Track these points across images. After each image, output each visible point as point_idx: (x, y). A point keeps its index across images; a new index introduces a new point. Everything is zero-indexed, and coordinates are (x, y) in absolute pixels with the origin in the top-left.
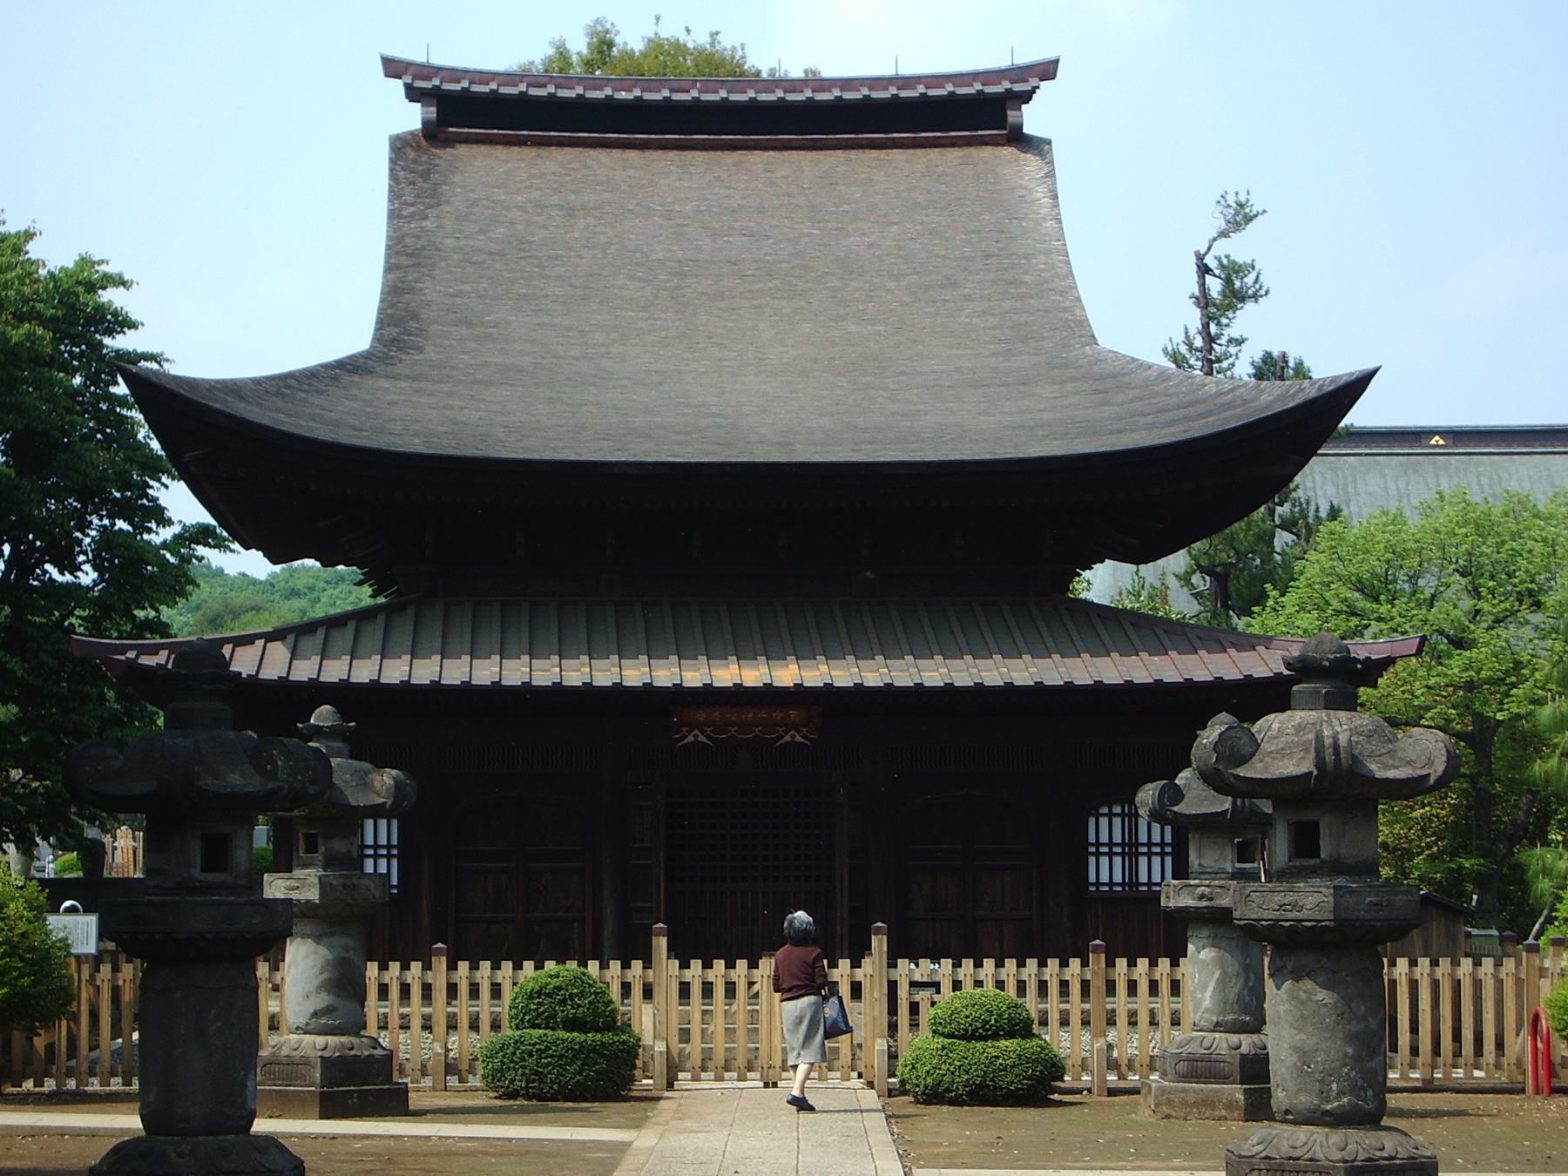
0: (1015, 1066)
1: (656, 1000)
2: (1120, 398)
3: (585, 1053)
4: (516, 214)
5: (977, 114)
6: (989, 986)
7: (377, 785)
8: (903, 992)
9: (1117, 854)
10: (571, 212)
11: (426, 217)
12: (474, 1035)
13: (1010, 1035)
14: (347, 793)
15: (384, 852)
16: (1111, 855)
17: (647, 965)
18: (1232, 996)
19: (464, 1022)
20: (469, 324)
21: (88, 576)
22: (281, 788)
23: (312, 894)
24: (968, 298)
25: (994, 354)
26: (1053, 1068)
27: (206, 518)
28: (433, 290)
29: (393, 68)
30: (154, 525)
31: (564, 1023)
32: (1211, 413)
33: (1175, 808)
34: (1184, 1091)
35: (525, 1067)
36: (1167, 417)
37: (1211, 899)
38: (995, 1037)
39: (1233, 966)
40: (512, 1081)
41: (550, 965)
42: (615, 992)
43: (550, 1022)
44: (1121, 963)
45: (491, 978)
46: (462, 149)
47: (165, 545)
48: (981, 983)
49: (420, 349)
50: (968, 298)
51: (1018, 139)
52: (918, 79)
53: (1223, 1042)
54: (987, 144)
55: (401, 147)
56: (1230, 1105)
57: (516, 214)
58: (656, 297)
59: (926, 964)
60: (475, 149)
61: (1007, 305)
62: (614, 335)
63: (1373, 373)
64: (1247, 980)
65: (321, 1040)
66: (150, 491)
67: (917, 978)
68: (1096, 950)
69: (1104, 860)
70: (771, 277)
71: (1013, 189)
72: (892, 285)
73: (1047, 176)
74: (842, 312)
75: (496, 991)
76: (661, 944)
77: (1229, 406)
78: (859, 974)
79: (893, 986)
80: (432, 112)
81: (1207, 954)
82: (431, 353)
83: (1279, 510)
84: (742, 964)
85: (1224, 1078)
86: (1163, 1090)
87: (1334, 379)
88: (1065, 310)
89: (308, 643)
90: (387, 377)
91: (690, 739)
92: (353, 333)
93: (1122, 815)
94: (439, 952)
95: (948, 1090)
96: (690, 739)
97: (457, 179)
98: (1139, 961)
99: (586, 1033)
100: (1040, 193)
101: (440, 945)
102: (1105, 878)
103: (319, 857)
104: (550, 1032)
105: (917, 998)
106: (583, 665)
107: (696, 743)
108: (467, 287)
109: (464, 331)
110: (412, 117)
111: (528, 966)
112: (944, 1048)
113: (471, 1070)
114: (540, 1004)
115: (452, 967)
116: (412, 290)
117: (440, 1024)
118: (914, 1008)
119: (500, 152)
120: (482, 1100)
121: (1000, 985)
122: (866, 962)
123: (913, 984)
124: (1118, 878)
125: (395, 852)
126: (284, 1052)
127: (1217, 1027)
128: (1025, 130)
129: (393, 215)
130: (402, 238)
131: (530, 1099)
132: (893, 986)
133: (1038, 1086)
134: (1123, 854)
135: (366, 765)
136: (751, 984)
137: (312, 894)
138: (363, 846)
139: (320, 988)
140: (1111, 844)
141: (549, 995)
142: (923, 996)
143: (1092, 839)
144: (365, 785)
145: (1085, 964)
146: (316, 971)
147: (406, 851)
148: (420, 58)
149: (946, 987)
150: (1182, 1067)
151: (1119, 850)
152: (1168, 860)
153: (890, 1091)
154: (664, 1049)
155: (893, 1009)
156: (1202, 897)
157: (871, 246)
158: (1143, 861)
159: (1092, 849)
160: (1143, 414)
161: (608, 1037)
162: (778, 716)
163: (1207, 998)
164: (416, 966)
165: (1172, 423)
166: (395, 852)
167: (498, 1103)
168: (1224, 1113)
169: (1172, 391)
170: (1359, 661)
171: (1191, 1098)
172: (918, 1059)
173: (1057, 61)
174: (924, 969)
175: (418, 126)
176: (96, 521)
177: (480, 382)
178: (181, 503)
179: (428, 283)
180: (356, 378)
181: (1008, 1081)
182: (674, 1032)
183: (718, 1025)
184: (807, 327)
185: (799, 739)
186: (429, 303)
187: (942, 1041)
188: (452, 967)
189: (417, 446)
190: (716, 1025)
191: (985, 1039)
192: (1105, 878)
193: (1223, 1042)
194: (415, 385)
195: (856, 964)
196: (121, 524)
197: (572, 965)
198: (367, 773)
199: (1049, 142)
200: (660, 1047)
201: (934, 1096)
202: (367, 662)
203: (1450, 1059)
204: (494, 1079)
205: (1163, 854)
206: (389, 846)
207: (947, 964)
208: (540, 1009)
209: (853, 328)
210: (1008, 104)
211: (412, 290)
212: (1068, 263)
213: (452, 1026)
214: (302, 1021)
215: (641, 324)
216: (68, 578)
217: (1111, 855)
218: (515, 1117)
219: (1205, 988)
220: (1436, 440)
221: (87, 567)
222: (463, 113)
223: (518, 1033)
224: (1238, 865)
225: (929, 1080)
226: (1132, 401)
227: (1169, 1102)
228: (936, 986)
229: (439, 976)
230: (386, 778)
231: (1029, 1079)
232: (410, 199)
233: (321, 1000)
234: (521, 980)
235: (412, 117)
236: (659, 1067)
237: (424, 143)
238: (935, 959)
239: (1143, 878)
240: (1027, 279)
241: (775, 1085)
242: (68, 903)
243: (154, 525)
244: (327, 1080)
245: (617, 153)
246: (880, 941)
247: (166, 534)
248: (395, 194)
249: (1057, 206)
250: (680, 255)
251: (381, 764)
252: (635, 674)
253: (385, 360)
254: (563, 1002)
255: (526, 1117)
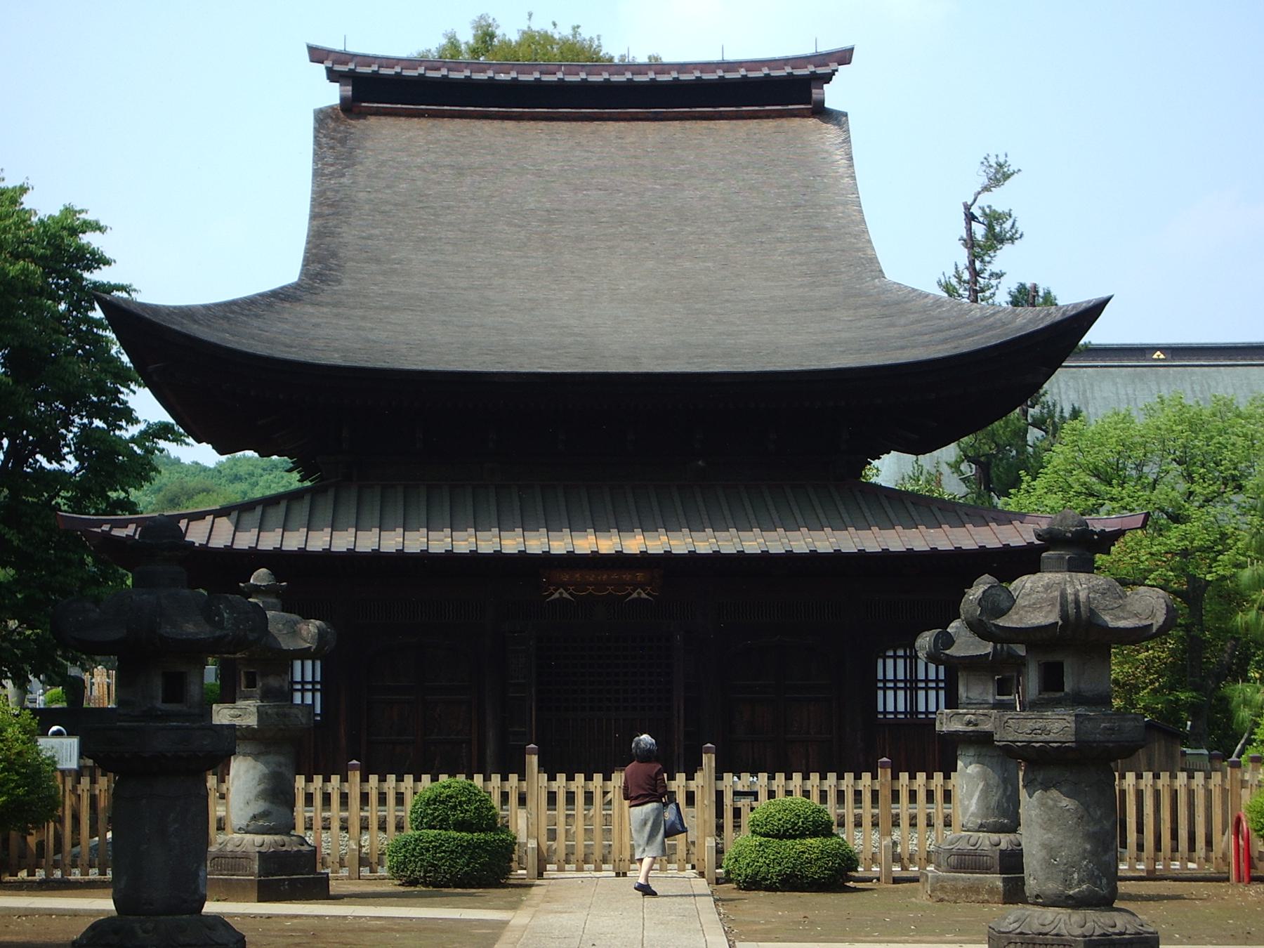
0: (818, 859)
1: (529, 806)
2: (903, 321)
3: (472, 849)
4: (416, 173)
5: (787, 92)
6: (798, 795)
7: (304, 633)
8: (728, 799)
9: (901, 688)
10: (460, 171)
11: (343, 175)
12: (382, 835)
13: (814, 834)
14: (280, 639)
15: (310, 687)
16: (895, 689)
17: (522, 778)
18: (993, 803)
19: (374, 824)
20: (378, 261)
21: (71, 464)
22: (227, 635)
23: (252, 721)
24: (781, 240)
25: (801, 286)
26: (849, 861)
27: (166, 417)
28: (349, 234)
29: (317, 55)
30: (124, 424)
31: (455, 825)
32: (976, 333)
33: (947, 652)
34: (955, 879)
35: (423, 860)
36: (941, 336)
37: (976, 725)
38: (802, 836)
39: (994, 778)
40: (413, 872)
41: (444, 778)
42: (496, 800)
43: (443, 824)
44: (904, 776)
45: (396, 788)
46: (372, 120)
47: (133, 439)
48: (791, 792)
49: (339, 282)
50: (781, 240)
51: (821, 112)
52: (740, 64)
53: (986, 840)
54: (795, 116)
55: (323, 118)
56: (991, 891)
57: (416, 173)
58: (529, 239)
59: (746, 777)
60: (383, 120)
61: (812, 246)
62: (495, 270)
63: (1107, 300)
64: (1005, 790)
65: (258, 839)
66: (121, 396)
67: (739, 788)
68: (884, 766)
69: (890, 694)
70: (622, 223)
71: (816, 153)
72: (719, 230)
73: (844, 142)
74: (678, 251)
75: (400, 799)
76: (533, 761)
77: (991, 327)
78: (693, 785)
79: (720, 795)
80: (349, 90)
81: (973, 769)
82: (347, 285)
83: (1031, 411)
84: (598, 777)
85: (986, 869)
86: (937, 879)
87: (1075, 306)
88: (858, 250)
89: (248, 518)
90: (312, 304)
91: (556, 595)
92: (285, 269)
93: (905, 657)
94: (354, 768)
95: (764, 879)
96: (556, 595)
97: (368, 144)
98: (918, 774)
99: (472, 833)
100: (839, 156)
101: (354, 762)
102: (890, 708)
103: (257, 690)
104: (443, 832)
105: (739, 805)
106: (470, 536)
107: (561, 599)
108: (377, 232)
109: (374, 267)
110: (332, 94)
111: (426, 778)
112: (761, 845)
113: (380, 863)
114: (435, 809)
115: (365, 779)
116: (332, 234)
117: (355, 826)
118: (737, 813)
119: (403, 122)
120: (389, 887)
121: (806, 794)
122: (698, 775)
123: (736, 793)
124: (901, 708)
125: (318, 687)
126: (229, 848)
127: (981, 828)
128: (826, 105)
129: (317, 174)
130: (324, 192)
131: (427, 886)
132: (720, 795)
133: (837, 875)
134: (905, 689)
135: (295, 617)
136: (605, 793)
137: (252, 721)
138: (293, 682)
139: (258, 797)
140: (895, 680)
141: (442, 802)
142: (744, 803)
143: (880, 676)
144: (294, 633)
145: (874, 777)
146: (255, 782)
147: (327, 686)
148: (338, 47)
149: (763, 796)
150: (953, 860)
151: (902, 685)
152: (942, 693)
153: (717, 879)
154: (535, 845)
155: (720, 813)
156: (969, 723)
157: (702, 198)
158: (921, 694)
159: (880, 685)
160: (921, 334)
161: (490, 836)
162: (627, 577)
163: (973, 805)
164: (335, 779)
165: (945, 341)
166: (318, 687)
167: (402, 889)
168: (986, 897)
169: (945, 315)
170: (1095, 533)
171: (960, 885)
172: (740, 854)
173: (852, 50)
174: (745, 781)
175: (337, 101)
176: (77, 420)
177: (387, 308)
178: (146, 406)
179: (345, 228)
180: (287, 305)
181: (813, 871)
182: (544, 832)
183: (579, 826)
184: (650, 264)
185: (644, 595)
186: (346, 244)
187: (759, 839)
188: (365, 779)
189: (336, 359)
190: (577, 826)
191: (794, 837)
192: (890, 708)
193: (986, 840)
194: (335, 310)
195: (690, 777)
196: (98, 423)
197: (461, 778)
198: (296, 623)
199: (846, 115)
200: (532, 844)
201: (753, 884)
202: (296, 534)
203: (1169, 854)
204: (398, 870)
205: (937, 689)
206: (313, 682)
207: (763, 777)
208: (435, 813)
209: (688, 264)
210: (813, 84)
211: (332, 234)
212: (861, 212)
213: (364, 827)
214: (243, 823)
215: (517, 261)
216: (55, 466)
217: (895, 689)
218: (415, 900)
219: (972, 797)
220: (1158, 355)
221: (70, 457)
222: (373, 91)
223: (418, 832)
224: (998, 697)
225: (749, 870)
226: (912, 323)
227: (943, 888)
228: (755, 795)
229: (354, 786)
230: (311, 628)
231: (830, 869)
232: (330, 160)
233: (259, 806)
234: (420, 790)
235: (332, 94)
236: (531, 860)
237: (342, 115)
238: (754, 773)
239: (922, 708)
240: (828, 225)
241: (625, 875)
242: (55, 728)
243: (124, 424)
244: (264, 871)
245: (497, 124)
246: (710, 759)
247: (134, 430)
248: (318, 157)
249: (852, 166)
250: (548, 205)
251: (307, 616)
252: (512, 543)
253: (311, 290)
254: (454, 808)
255: (424, 900)
